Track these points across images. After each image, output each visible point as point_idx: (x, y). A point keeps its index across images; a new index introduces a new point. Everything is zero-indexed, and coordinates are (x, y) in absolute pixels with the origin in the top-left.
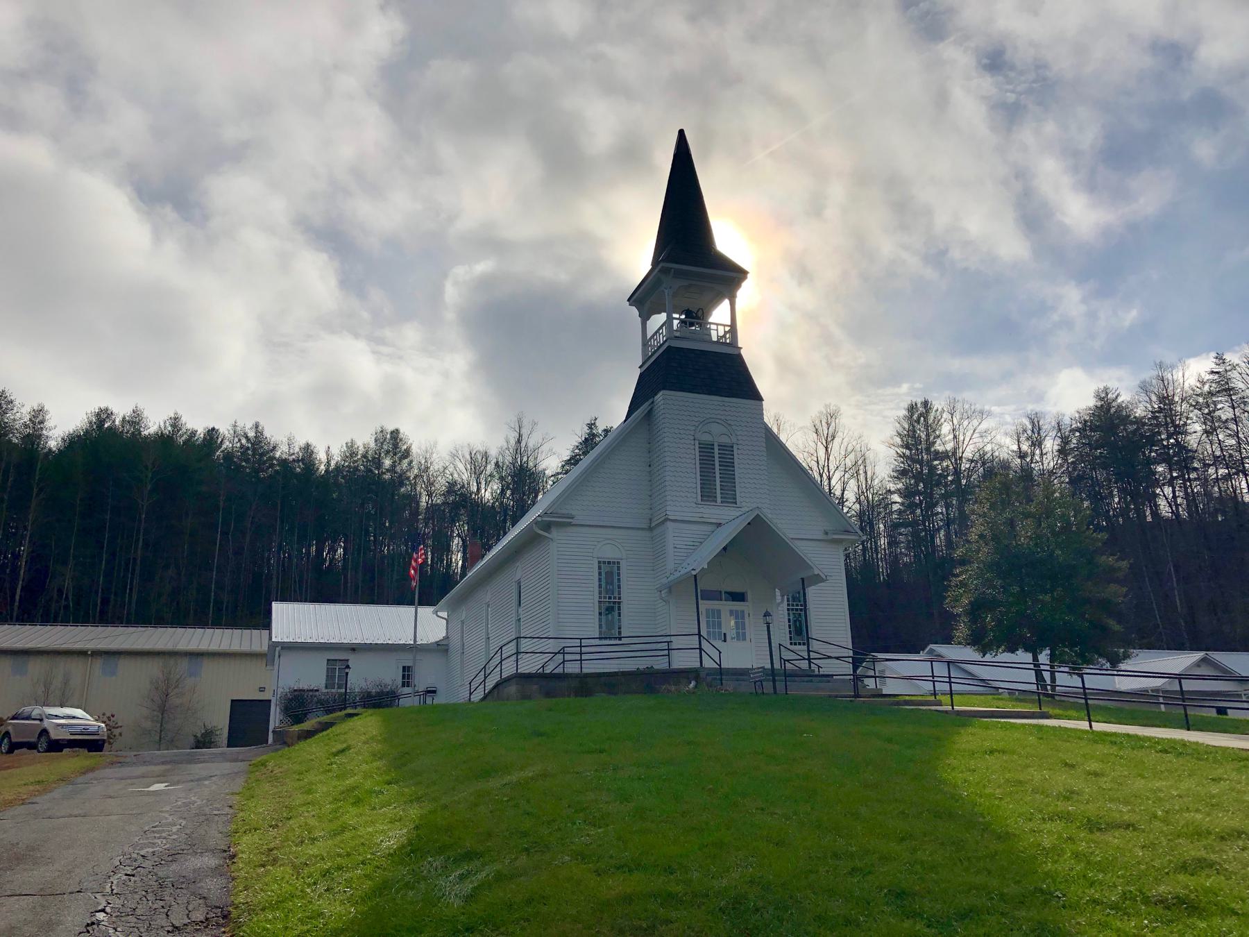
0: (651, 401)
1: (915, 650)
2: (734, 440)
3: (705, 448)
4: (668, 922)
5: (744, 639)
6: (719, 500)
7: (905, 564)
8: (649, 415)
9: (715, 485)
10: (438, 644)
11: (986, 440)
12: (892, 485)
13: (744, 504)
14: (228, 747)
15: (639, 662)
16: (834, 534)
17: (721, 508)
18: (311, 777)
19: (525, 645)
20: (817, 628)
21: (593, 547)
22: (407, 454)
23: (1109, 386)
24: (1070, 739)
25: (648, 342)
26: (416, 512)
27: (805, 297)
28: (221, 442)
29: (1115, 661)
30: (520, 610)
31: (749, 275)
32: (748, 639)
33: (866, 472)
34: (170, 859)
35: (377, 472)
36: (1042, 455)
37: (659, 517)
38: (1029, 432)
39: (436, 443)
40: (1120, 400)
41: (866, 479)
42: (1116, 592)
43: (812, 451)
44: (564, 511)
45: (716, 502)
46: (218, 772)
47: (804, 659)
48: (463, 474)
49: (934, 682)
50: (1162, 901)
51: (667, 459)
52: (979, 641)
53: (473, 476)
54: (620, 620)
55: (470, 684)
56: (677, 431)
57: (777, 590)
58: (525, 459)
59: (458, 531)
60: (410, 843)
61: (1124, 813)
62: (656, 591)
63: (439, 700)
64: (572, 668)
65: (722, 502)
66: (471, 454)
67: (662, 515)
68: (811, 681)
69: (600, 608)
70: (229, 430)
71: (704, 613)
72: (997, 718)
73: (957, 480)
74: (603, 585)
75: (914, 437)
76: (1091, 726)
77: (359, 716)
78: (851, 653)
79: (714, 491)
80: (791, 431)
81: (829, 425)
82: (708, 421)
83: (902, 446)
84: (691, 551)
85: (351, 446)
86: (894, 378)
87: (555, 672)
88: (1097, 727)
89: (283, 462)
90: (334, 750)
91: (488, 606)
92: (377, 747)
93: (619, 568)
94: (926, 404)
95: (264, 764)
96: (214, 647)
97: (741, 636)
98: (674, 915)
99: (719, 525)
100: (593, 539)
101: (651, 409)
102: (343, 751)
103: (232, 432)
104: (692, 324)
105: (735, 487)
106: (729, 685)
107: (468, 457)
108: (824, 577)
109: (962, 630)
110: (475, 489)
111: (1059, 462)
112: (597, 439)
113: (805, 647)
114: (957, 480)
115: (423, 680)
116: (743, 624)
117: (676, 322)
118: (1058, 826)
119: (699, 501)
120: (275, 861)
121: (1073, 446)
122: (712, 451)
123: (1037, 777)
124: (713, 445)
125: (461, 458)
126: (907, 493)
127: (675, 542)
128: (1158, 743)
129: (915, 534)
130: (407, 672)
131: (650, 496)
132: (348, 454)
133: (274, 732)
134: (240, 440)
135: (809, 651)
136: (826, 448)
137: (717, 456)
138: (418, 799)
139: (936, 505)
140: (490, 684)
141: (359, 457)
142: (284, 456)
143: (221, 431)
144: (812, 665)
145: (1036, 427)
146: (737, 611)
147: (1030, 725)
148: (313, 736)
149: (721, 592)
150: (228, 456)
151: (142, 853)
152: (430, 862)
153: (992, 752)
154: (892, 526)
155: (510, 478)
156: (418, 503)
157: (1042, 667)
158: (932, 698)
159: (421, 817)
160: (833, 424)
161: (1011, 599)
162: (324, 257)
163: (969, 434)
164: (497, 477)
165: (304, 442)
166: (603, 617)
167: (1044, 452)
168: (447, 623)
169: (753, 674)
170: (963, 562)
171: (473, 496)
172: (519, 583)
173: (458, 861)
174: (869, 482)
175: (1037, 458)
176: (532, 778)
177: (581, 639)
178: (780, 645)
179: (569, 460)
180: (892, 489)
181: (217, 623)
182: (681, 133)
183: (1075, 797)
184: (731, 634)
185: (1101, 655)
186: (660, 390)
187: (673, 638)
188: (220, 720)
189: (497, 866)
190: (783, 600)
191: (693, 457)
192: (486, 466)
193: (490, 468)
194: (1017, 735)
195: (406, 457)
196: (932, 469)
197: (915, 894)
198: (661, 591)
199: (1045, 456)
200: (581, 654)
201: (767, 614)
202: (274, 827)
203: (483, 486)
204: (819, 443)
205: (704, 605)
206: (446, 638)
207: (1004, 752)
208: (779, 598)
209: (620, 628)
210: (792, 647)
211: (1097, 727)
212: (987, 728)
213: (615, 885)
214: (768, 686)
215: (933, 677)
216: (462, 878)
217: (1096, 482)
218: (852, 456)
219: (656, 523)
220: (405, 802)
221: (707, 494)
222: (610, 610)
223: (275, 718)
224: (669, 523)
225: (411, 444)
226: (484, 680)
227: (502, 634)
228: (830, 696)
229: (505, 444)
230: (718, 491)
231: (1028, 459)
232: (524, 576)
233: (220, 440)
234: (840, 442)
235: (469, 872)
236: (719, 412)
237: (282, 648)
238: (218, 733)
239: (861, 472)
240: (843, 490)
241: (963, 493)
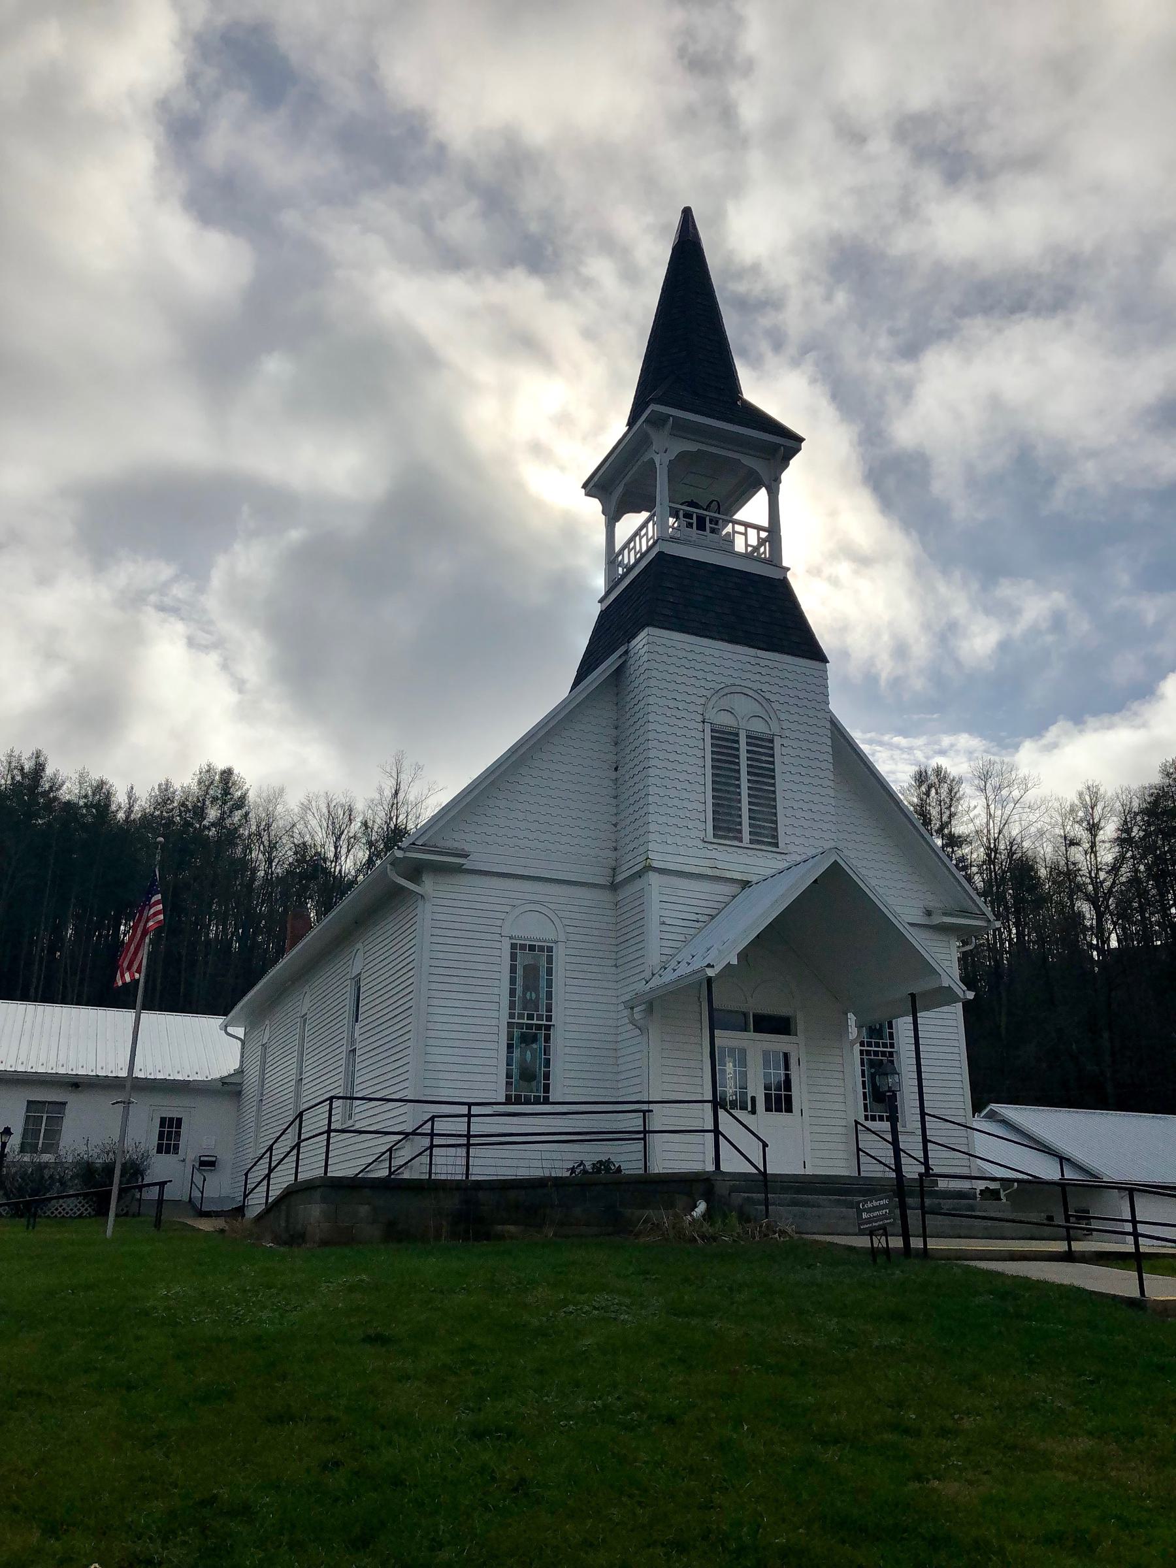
0: (622, 649)
2: (775, 729)
5: (789, 1110)
6: (746, 836)
8: (619, 672)
9: (740, 809)
10: (223, 1081)
13: (791, 848)
16: (945, 914)
17: (750, 852)
21: (503, 916)
22: (241, 803)
25: (618, 555)
37: (631, 863)
44: (450, 844)
45: (776, 845)
48: (318, 836)
55: (246, 1175)
56: (672, 704)
57: (850, 1015)
58: (401, 817)
62: (622, 1007)
65: (751, 842)
66: (328, 806)
67: (640, 859)
69: (510, 1037)
74: (519, 992)
79: (738, 820)
82: (726, 691)
84: (692, 931)
85: (165, 788)
89: (68, 803)
93: (550, 960)
99: (746, 884)
100: (503, 901)
101: (625, 662)
105: (775, 814)
107: (325, 810)
110: (331, 855)
115: (194, 1141)
119: (710, 838)
122: (736, 745)
124: (737, 735)
125: (315, 810)
127: (663, 913)
131: (615, 825)
132: (160, 800)
137: (743, 755)
141: (175, 804)
164: (364, 841)
168: (243, 1048)
169: (869, 1210)
172: (357, 980)
182: (687, 213)
186: (642, 628)
187: (651, 1107)
191: (700, 754)
193: (356, 826)
198: (632, 1008)
203: (344, 851)
205: (725, 1038)
206: (240, 1072)
210: (869, 1124)
219: (626, 875)
224: (653, 877)
225: (248, 790)
226: (268, 1176)
229: (377, 796)
232: (366, 968)
236: (749, 675)
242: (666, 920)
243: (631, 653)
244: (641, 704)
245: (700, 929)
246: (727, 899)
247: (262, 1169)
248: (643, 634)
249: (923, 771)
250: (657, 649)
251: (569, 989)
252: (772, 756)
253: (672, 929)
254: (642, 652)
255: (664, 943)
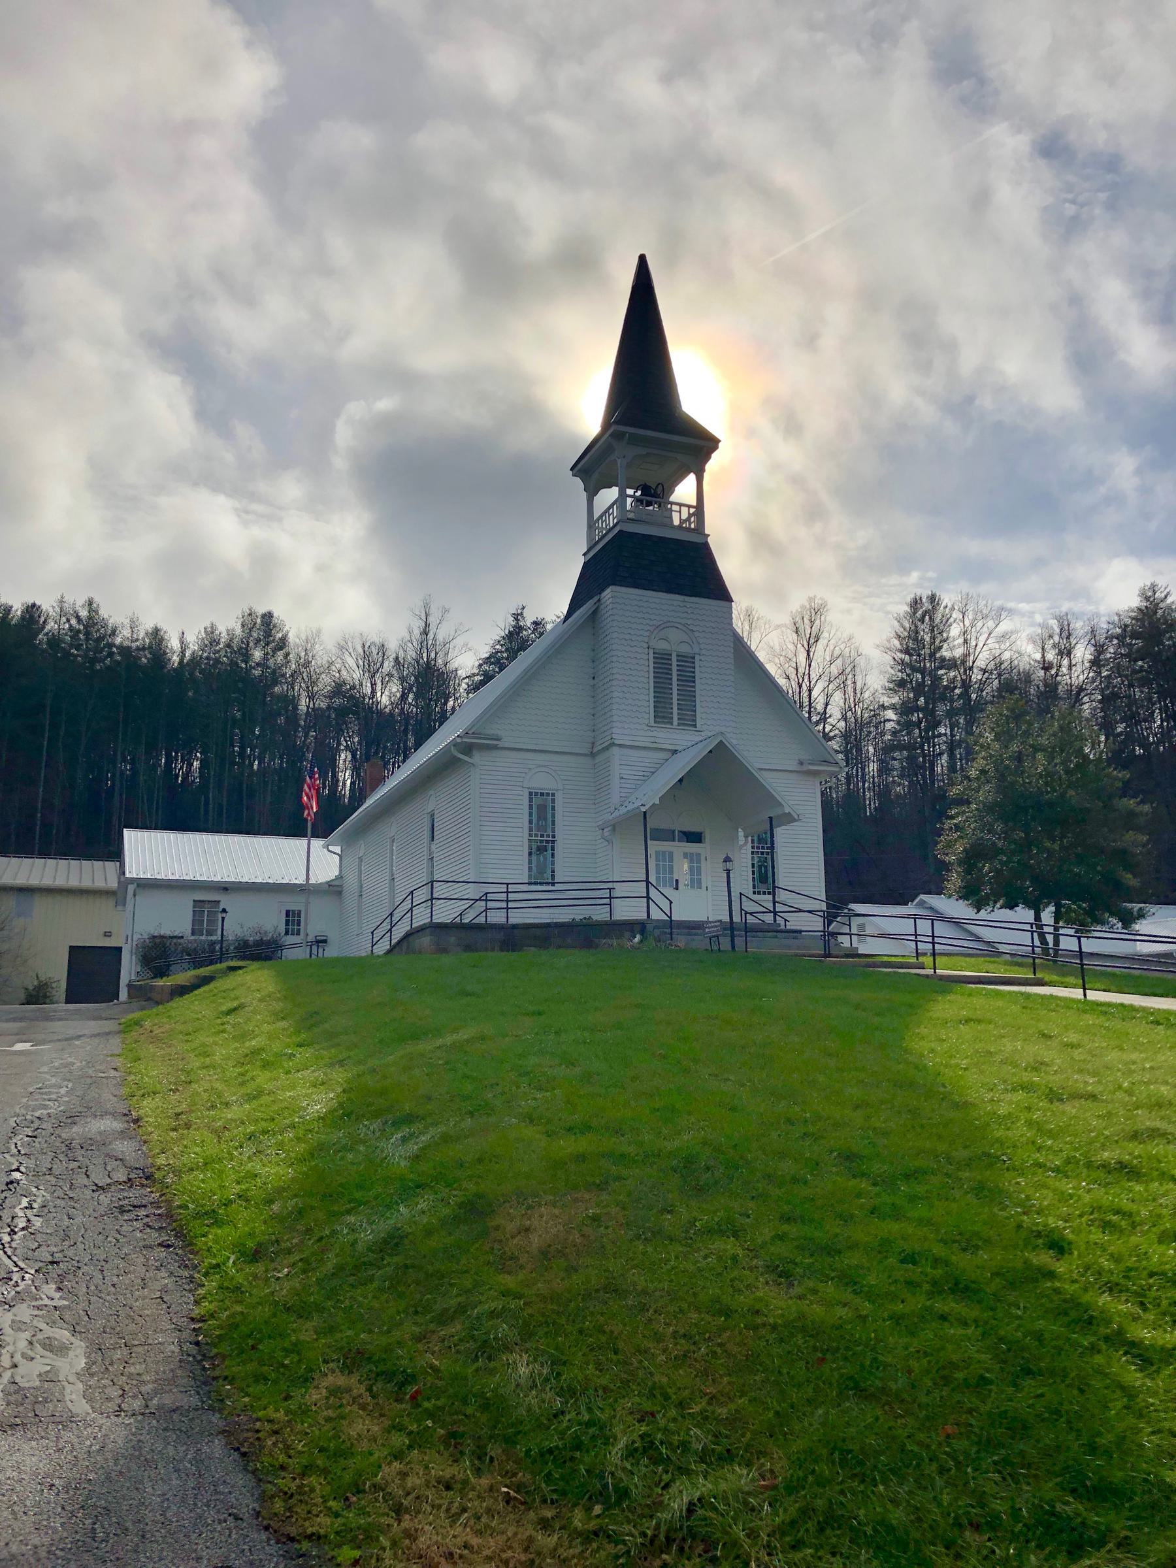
0: (596, 599)
1: (901, 899)
2: (696, 650)
3: (662, 673)
4: (619, 1178)
6: (675, 721)
7: (898, 796)
8: (595, 612)
9: (672, 704)
10: (329, 884)
11: (1003, 647)
12: (886, 699)
13: (705, 727)
14: (68, 1002)
15: (575, 912)
18: (202, 1038)
19: (440, 890)
20: (784, 875)
22: (282, 644)
23: (1157, 582)
24: (1058, 1009)
26: (293, 717)
27: (791, 454)
28: (44, 622)
29: (1128, 920)
30: (433, 847)
31: (720, 445)
32: (704, 886)
33: (854, 683)
34: (69, 1121)
35: (243, 666)
36: (1070, 666)
37: (603, 740)
38: (1056, 638)
39: (319, 632)
40: (1169, 600)
41: (855, 690)
42: (1135, 841)
43: (791, 655)
46: (86, 1032)
47: (771, 912)
48: (353, 673)
49: (916, 942)
50: (1105, 1166)
51: (614, 671)
52: (973, 894)
53: (366, 674)
54: (553, 863)
56: (627, 637)
59: (346, 741)
60: (341, 1105)
61: (1090, 1084)
63: (331, 952)
64: (497, 918)
66: (364, 646)
67: (607, 739)
68: (776, 937)
69: (530, 848)
70: (53, 607)
71: (654, 856)
72: (983, 984)
73: (965, 695)
75: (916, 640)
76: (1085, 995)
77: (244, 970)
78: (824, 907)
80: (765, 629)
81: (812, 622)
83: (901, 651)
84: (639, 782)
85: (211, 631)
86: (902, 562)
87: (476, 921)
88: (1092, 995)
89: (125, 650)
90: (224, 1008)
91: (393, 841)
92: (279, 1006)
93: (553, 801)
94: (933, 598)
95: (138, 1023)
96: (47, 882)
97: (696, 883)
98: (625, 1172)
99: (675, 752)
102: (235, 1009)
103: (58, 609)
104: (649, 504)
105: (695, 706)
106: (681, 941)
107: (360, 651)
108: (796, 817)
109: (955, 880)
110: (369, 691)
111: (1091, 675)
112: (524, 632)
113: (770, 897)
114: (965, 695)
115: (314, 926)
116: (699, 868)
117: (629, 500)
118: (1020, 1095)
120: (188, 1126)
121: (1108, 656)
123: (1009, 1047)
124: (671, 655)
125: (351, 651)
126: (905, 709)
128: (1152, 1014)
129: (911, 759)
130: (293, 920)
132: (207, 642)
133: (129, 986)
134: (68, 620)
135: (774, 903)
136: (808, 652)
137: (674, 668)
138: (341, 1063)
139: (938, 724)
140: (398, 934)
142: (127, 643)
143: (44, 607)
144: (778, 917)
145: (1066, 632)
146: (692, 854)
147: (1010, 992)
148: (192, 991)
149: (674, 832)
150: (54, 641)
151: (37, 1114)
152: (366, 1126)
153: (967, 1021)
154: (883, 749)
155: (413, 678)
156: (296, 708)
157: (1046, 929)
158: (914, 960)
159: (348, 1081)
160: (817, 622)
161: (1013, 847)
162: (175, 381)
163: (982, 639)
165: (152, 626)
166: (534, 858)
167: (1073, 662)
168: (341, 860)
169: (709, 928)
170: (962, 801)
171: (367, 700)
172: (432, 816)
173: (397, 1124)
174: (859, 695)
175: (1064, 670)
176: (468, 1041)
177: (508, 884)
178: (741, 894)
179: (487, 658)
180: (886, 704)
181: (45, 852)
182: (642, 259)
183: (1043, 1068)
184: (684, 880)
185: (1112, 914)
188: (57, 972)
189: (442, 1129)
190: (746, 842)
191: (646, 669)
192: (383, 663)
193: (388, 666)
194: (1000, 1003)
195: (281, 648)
196: (936, 679)
197: (864, 1157)
199: (1074, 668)
200: (507, 901)
201: (727, 860)
202: (175, 1091)
204: (799, 646)
206: (340, 877)
207: (979, 1021)
208: (742, 840)
209: (553, 871)
210: (756, 897)
211: (1092, 995)
212: (970, 995)
213: (568, 1146)
214: (725, 943)
215: (916, 935)
216: (404, 1140)
217: (1132, 701)
218: (839, 662)
219: (600, 748)
220: (325, 1065)
221: (661, 715)
222: (541, 850)
223: (129, 969)
224: (615, 750)
226: (390, 930)
227: (413, 878)
228: (796, 955)
230: (675, 711)
231: (1053, 672)
233: (42, 619)
234: (825, 644)
235: (412, 1135)
237: (138, 885)
238: (54, 985)
239: (849, 682)
240: (827, 704)
241: (972, 710)
242: (625, 777)
243: (602, 601)
244: (608, 638)
245: (645, 781)
246: (663, 761)
247: (386, 926)
248: (608, 590)
249: (918, 598)
250: (618, 600)
251: (565, 818)
252: (694, 668)
253: (629, 781)
254: (609, 602)
255: (622, 790)
